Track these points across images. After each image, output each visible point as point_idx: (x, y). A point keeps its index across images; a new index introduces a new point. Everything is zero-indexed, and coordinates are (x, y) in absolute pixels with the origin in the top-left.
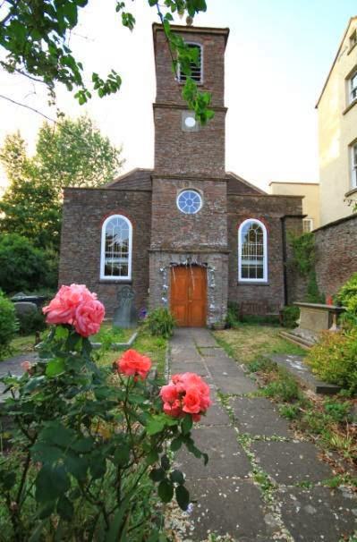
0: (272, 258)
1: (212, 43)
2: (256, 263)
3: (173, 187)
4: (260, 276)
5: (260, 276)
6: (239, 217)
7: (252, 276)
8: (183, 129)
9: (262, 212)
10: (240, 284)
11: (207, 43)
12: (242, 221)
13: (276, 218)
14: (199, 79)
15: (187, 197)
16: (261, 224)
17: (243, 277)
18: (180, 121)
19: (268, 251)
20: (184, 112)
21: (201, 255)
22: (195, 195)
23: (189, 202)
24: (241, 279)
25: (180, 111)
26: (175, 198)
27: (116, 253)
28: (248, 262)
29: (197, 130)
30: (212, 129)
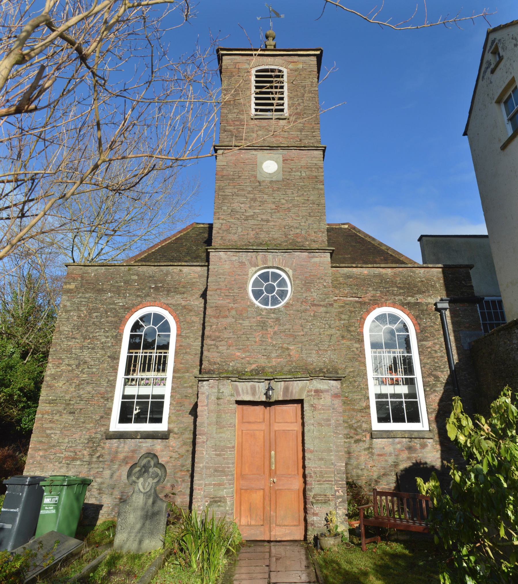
0: (431, 379)
1: (300, 66)
2: (403, 389)
3: (242, 264)
4: (414, 417)
5: (414, 417)
6: (363, 304)
7: (399, 419)
8: (260, 178)
9: (403, 294)
10: (373, 435)
11: (291, 66)
12: (368, 312)
13: (427, 304)
14: (282, 110)
15: (279, 285)
16: (378, 311)
17: (159, 420)
18: (255, 165)
19: (423, 365)
20: (260, 154)
21: (38, 135)
22: (279, 276)
23: (270, 289)
24: (377, 426)
25: (254, 152)
26: (246, 283)
27: (160, 354)
28: (389, 390)
29: (280, 177)
30: (304, 174)
